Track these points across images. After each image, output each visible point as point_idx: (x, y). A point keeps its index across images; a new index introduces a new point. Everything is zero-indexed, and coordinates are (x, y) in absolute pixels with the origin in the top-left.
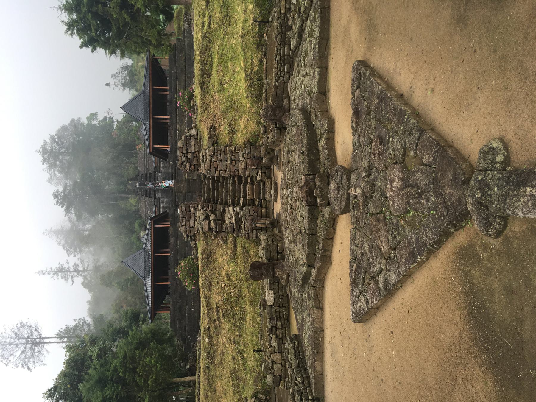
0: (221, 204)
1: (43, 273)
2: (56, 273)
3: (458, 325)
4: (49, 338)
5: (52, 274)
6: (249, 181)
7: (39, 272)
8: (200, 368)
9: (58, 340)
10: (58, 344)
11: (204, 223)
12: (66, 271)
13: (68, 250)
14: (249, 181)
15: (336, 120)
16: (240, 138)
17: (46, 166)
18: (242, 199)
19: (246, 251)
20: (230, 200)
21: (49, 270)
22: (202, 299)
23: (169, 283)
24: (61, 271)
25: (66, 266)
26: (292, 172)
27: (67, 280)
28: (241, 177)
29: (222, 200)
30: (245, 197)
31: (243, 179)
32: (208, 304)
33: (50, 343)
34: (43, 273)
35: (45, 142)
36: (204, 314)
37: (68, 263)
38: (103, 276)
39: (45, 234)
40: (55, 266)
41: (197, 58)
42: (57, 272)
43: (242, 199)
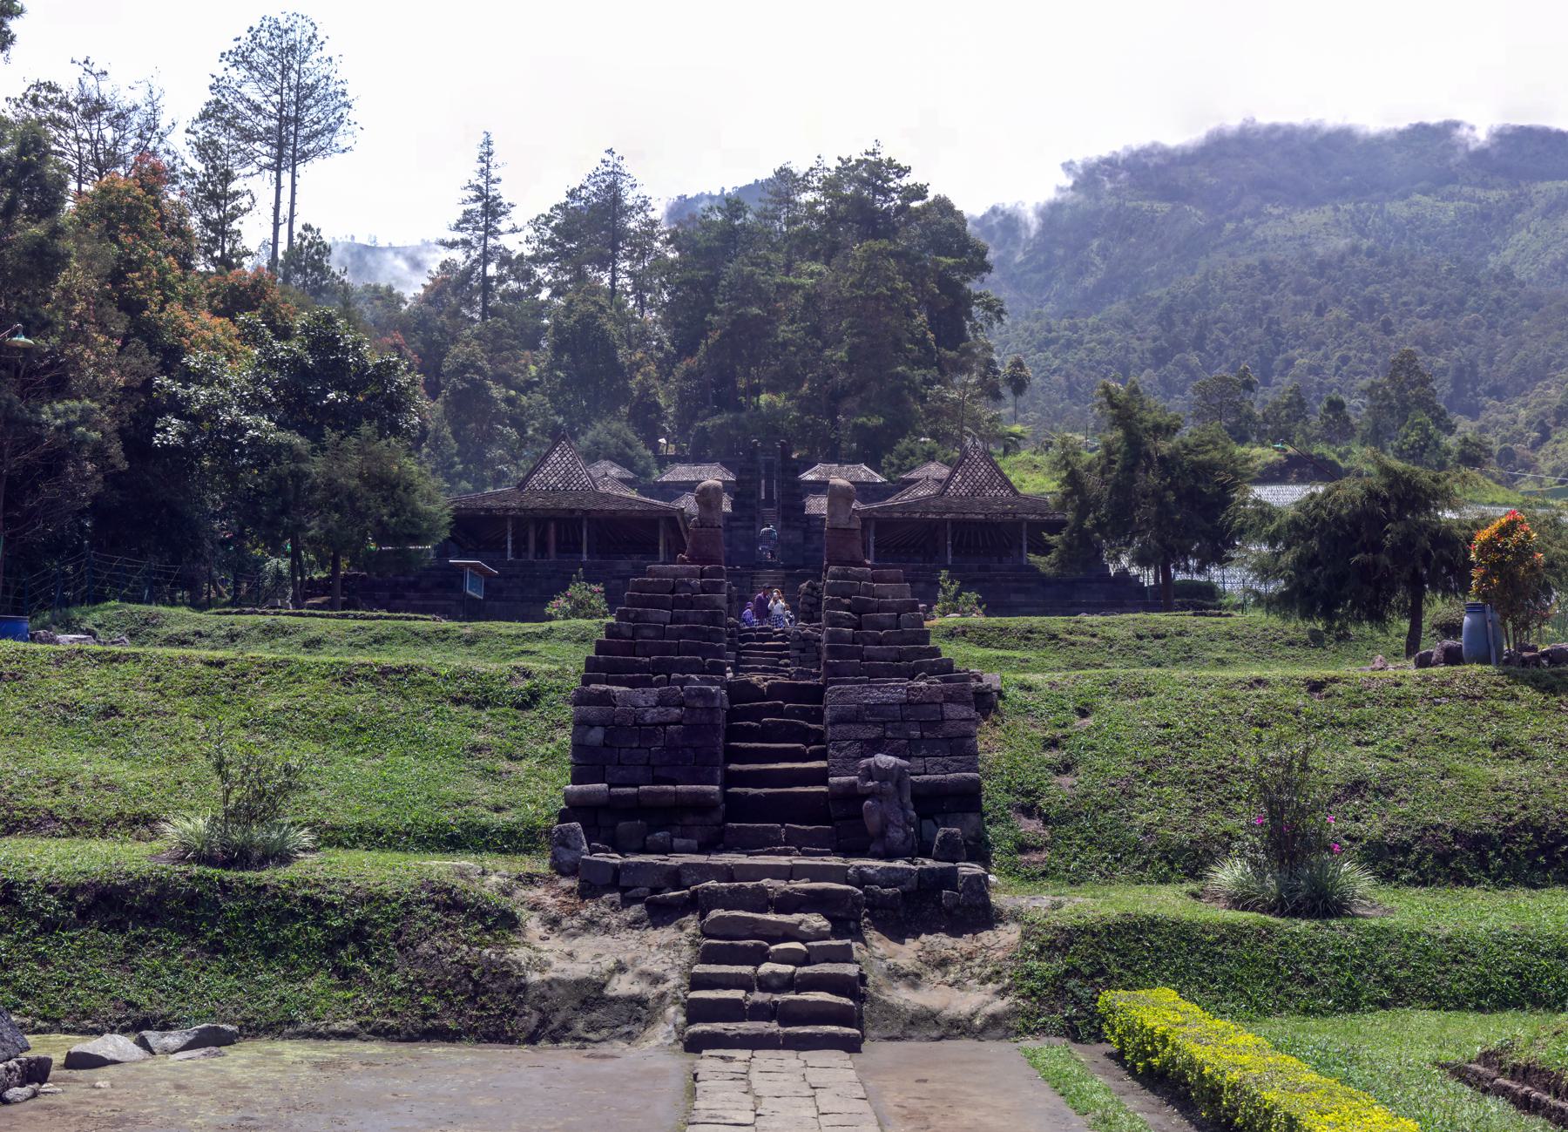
0: (739, 662)
1: (486, 156)
2: (482, 195)
4: (294, 185)
5: (481, 182)
7: (489, 143)
8: (409, 619)
10: (297, 189)
12: (487, 226)
13: (549, 219)
15: (1415, 122)
17: (833, 164)
21: (494, 174)
23: (585, 556)
24: (489, 209)
25: (504, 225)
26: (1194, 359)
27: (457, 228)
29: (745, 662)
32: (539, 637)
33: (279, 188)
34: (486, 156)
35: (902, 171)
36: (417, 656)
37: (514, 231)
38: (650, 916)
39: (608, 157)
40: (504, 192)
41: (1035, 621)
42: (487, 197)
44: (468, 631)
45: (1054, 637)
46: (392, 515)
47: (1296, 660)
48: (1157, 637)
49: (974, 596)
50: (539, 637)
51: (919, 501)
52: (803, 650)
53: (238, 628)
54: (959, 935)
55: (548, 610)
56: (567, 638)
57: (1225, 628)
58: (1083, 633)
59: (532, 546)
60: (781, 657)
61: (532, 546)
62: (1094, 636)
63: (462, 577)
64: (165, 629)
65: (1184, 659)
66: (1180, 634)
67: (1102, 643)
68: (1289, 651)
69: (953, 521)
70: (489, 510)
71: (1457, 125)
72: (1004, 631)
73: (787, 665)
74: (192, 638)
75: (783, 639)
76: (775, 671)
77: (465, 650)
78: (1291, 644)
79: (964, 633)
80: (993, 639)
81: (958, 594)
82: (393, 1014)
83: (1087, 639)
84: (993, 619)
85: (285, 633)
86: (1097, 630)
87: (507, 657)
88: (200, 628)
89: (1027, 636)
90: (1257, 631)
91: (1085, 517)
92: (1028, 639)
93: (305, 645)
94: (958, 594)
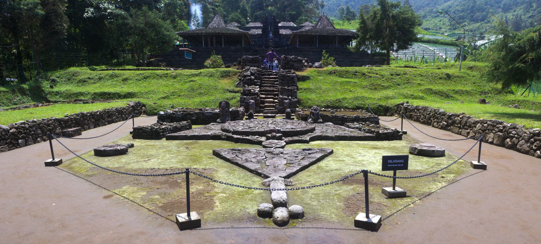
0: (261, 83)
3: (257, 199)
6: (276, 101)
8: (155, 70)
9: (159, 211)
11: (249, 72)
14: (276, 101)
15: (160, 141)
16: (301, 95)
18: (264, 96)
19: (233, 98)
20: (263, 89)
22: (199, 71)
28: (278, 96)
30: (266, 98)
31: (277, 97)
32: (197, 75)
41: (357, 68)
43: (264, 96)
44: (174, 74)
45: (364, 74)
46: (155, 36)
47: (443, 84)
48: (398, 75)
49: (333, 58)
50: (197, 75)
51: (306, 31)
52: (283, 80)
53: (102, 76)
54: (361, 66)
55: (206, 64)
56: (206, 75)
57: (419, 72)
58: (373, 73)
59: (209, 43)
60: (275, 81)
61: (209, 43)
62: (377, 74)
63: (184, 54)
64: (79, 77)
65: (407, 83)
66: (404, 74)
67: (380, 77)
68: (441, 81)
69: (319, 36)
70: (197, 33)
71: (387, 198)
72: (347, 72)
73: (277, 84)
74: (87, 80)
75: (276, 75)
76: (274, 87)
77: (173, 80)
78: (441, 78)
79: (335, 73)
80: (344, 75)
81: (328, 58)
82: (359, 153)
83: (375, 75)
84: (344, 68)
85: (117, 77)
86: (378, 72)
87: (186, 82)
88: (90, 76)
89: (355, 74)
90: (429, 74)
91: (367, 34)
92: (355, 75)
93: (123, 81)
94: (328, 58)
